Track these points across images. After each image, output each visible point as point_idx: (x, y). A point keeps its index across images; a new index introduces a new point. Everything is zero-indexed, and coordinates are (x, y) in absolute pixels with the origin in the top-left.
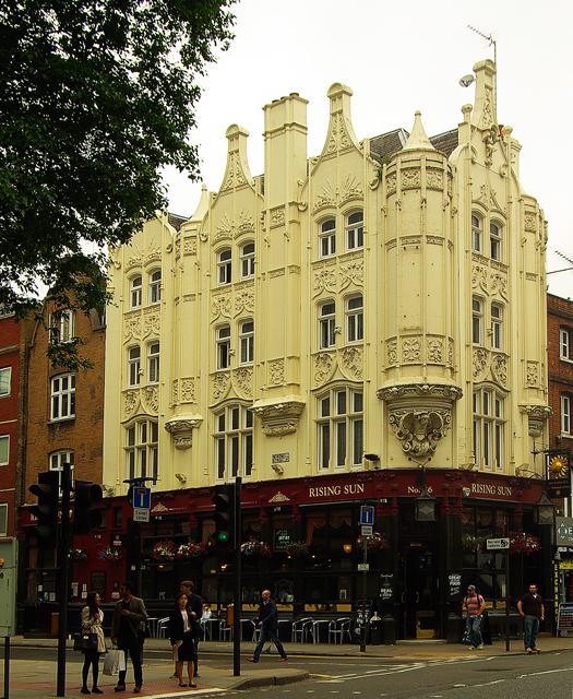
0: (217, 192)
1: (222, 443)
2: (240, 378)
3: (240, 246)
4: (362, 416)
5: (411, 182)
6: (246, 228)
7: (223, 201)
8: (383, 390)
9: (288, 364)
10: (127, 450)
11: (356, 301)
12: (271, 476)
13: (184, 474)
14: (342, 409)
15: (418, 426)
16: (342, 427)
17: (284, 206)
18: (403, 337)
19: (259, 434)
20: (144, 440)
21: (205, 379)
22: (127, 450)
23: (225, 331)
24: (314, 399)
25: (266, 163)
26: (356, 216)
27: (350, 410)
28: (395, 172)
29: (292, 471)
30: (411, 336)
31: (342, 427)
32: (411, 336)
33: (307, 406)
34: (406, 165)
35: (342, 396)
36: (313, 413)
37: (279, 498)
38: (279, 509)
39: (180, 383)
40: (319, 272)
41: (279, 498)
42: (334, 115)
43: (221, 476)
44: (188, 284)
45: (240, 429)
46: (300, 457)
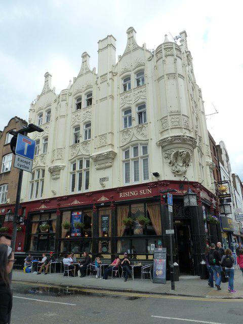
0: (76, 77)
1: (33, 184)
2: (84, 146)
3: (85, 94)
4: (89, 169)
5: (169, 53)
6: (89, 87)
7: (78, 80)
8: (162, 140)
9: (109, 136)
10: (31, 182)
11: (88, 125)
12: (99, 188)
13: (55, 190)
14: (136, 153)
15: (179, 158)
16: (136, 163)
17: (107, 74)
18: (170, 115)
19: (92, 169)
20: (38, 177)
21: (67, 149)
22: (31, 182)
23: (77, 128)
24: (121, 151)
25: (99, 61)
26: (140, 73)
27: (41, 177)
28: (161, 50)
29: (109, 185)
30: (175, 115)
31: (136, 163)
32: (175, 115)
33: (118, 154)
34: (166, 47)
35: (81, 162)
36: (121, 156)
37: (43, 207)
38: (43, 211)
39: (56, 151)
40: (123, 97)
41: (103, 199)
42: (83, 62)
43: (36, 197)
44: (62, 111)
45: (139, 156)
46: (115, 178)
